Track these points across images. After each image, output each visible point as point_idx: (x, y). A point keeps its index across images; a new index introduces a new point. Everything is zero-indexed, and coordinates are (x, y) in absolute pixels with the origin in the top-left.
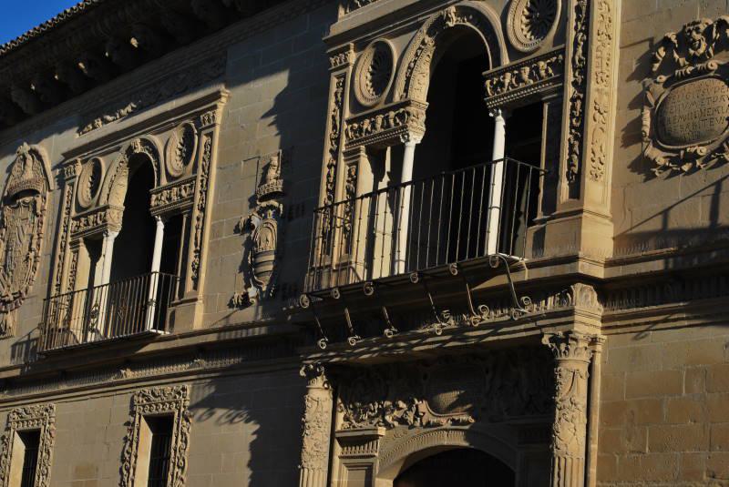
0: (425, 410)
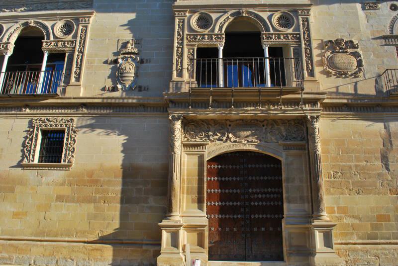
0: (232, 137)
